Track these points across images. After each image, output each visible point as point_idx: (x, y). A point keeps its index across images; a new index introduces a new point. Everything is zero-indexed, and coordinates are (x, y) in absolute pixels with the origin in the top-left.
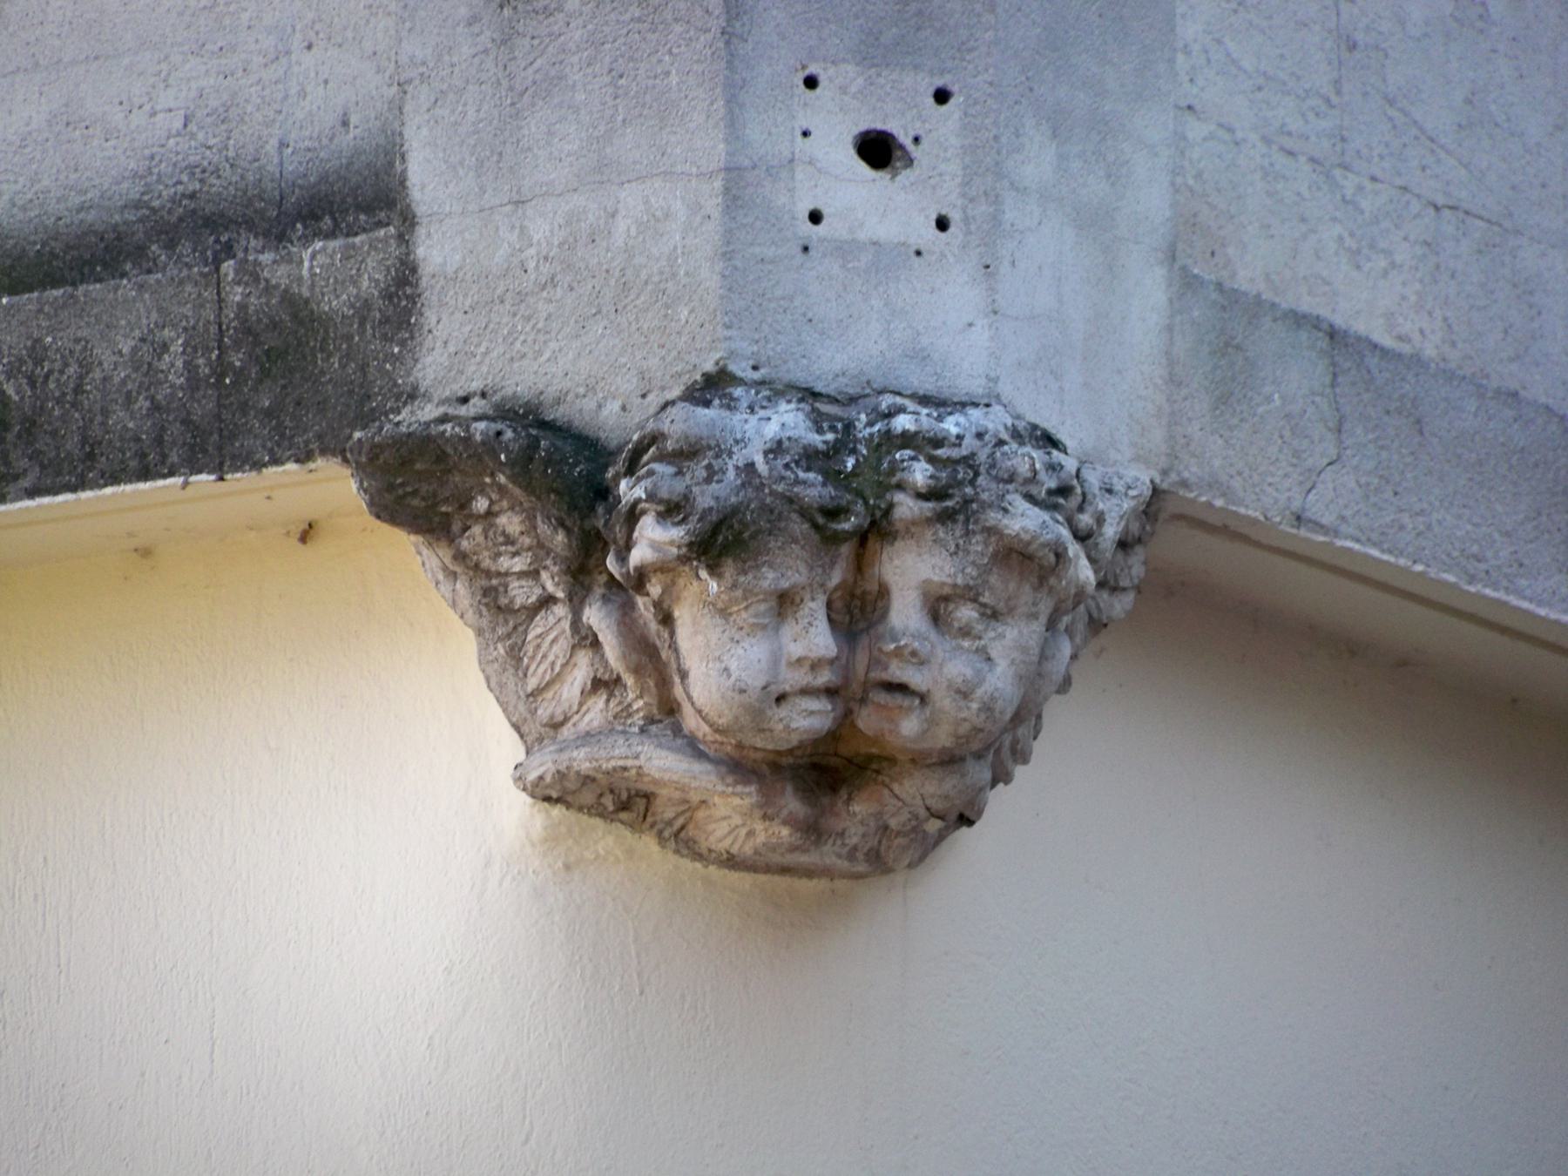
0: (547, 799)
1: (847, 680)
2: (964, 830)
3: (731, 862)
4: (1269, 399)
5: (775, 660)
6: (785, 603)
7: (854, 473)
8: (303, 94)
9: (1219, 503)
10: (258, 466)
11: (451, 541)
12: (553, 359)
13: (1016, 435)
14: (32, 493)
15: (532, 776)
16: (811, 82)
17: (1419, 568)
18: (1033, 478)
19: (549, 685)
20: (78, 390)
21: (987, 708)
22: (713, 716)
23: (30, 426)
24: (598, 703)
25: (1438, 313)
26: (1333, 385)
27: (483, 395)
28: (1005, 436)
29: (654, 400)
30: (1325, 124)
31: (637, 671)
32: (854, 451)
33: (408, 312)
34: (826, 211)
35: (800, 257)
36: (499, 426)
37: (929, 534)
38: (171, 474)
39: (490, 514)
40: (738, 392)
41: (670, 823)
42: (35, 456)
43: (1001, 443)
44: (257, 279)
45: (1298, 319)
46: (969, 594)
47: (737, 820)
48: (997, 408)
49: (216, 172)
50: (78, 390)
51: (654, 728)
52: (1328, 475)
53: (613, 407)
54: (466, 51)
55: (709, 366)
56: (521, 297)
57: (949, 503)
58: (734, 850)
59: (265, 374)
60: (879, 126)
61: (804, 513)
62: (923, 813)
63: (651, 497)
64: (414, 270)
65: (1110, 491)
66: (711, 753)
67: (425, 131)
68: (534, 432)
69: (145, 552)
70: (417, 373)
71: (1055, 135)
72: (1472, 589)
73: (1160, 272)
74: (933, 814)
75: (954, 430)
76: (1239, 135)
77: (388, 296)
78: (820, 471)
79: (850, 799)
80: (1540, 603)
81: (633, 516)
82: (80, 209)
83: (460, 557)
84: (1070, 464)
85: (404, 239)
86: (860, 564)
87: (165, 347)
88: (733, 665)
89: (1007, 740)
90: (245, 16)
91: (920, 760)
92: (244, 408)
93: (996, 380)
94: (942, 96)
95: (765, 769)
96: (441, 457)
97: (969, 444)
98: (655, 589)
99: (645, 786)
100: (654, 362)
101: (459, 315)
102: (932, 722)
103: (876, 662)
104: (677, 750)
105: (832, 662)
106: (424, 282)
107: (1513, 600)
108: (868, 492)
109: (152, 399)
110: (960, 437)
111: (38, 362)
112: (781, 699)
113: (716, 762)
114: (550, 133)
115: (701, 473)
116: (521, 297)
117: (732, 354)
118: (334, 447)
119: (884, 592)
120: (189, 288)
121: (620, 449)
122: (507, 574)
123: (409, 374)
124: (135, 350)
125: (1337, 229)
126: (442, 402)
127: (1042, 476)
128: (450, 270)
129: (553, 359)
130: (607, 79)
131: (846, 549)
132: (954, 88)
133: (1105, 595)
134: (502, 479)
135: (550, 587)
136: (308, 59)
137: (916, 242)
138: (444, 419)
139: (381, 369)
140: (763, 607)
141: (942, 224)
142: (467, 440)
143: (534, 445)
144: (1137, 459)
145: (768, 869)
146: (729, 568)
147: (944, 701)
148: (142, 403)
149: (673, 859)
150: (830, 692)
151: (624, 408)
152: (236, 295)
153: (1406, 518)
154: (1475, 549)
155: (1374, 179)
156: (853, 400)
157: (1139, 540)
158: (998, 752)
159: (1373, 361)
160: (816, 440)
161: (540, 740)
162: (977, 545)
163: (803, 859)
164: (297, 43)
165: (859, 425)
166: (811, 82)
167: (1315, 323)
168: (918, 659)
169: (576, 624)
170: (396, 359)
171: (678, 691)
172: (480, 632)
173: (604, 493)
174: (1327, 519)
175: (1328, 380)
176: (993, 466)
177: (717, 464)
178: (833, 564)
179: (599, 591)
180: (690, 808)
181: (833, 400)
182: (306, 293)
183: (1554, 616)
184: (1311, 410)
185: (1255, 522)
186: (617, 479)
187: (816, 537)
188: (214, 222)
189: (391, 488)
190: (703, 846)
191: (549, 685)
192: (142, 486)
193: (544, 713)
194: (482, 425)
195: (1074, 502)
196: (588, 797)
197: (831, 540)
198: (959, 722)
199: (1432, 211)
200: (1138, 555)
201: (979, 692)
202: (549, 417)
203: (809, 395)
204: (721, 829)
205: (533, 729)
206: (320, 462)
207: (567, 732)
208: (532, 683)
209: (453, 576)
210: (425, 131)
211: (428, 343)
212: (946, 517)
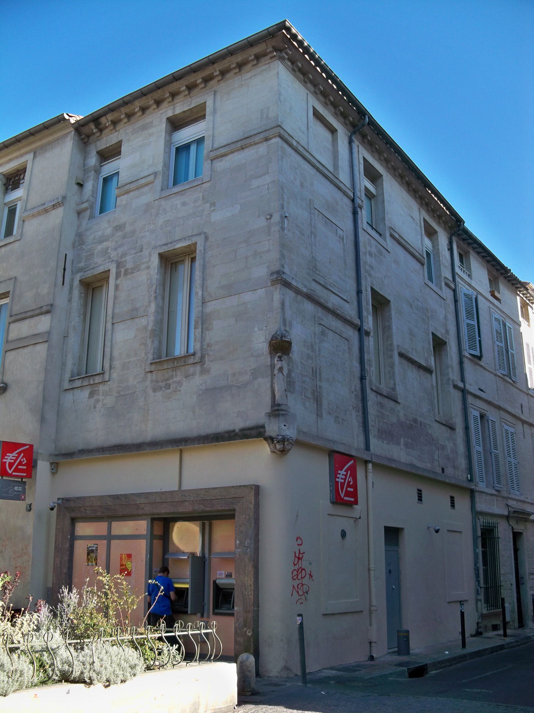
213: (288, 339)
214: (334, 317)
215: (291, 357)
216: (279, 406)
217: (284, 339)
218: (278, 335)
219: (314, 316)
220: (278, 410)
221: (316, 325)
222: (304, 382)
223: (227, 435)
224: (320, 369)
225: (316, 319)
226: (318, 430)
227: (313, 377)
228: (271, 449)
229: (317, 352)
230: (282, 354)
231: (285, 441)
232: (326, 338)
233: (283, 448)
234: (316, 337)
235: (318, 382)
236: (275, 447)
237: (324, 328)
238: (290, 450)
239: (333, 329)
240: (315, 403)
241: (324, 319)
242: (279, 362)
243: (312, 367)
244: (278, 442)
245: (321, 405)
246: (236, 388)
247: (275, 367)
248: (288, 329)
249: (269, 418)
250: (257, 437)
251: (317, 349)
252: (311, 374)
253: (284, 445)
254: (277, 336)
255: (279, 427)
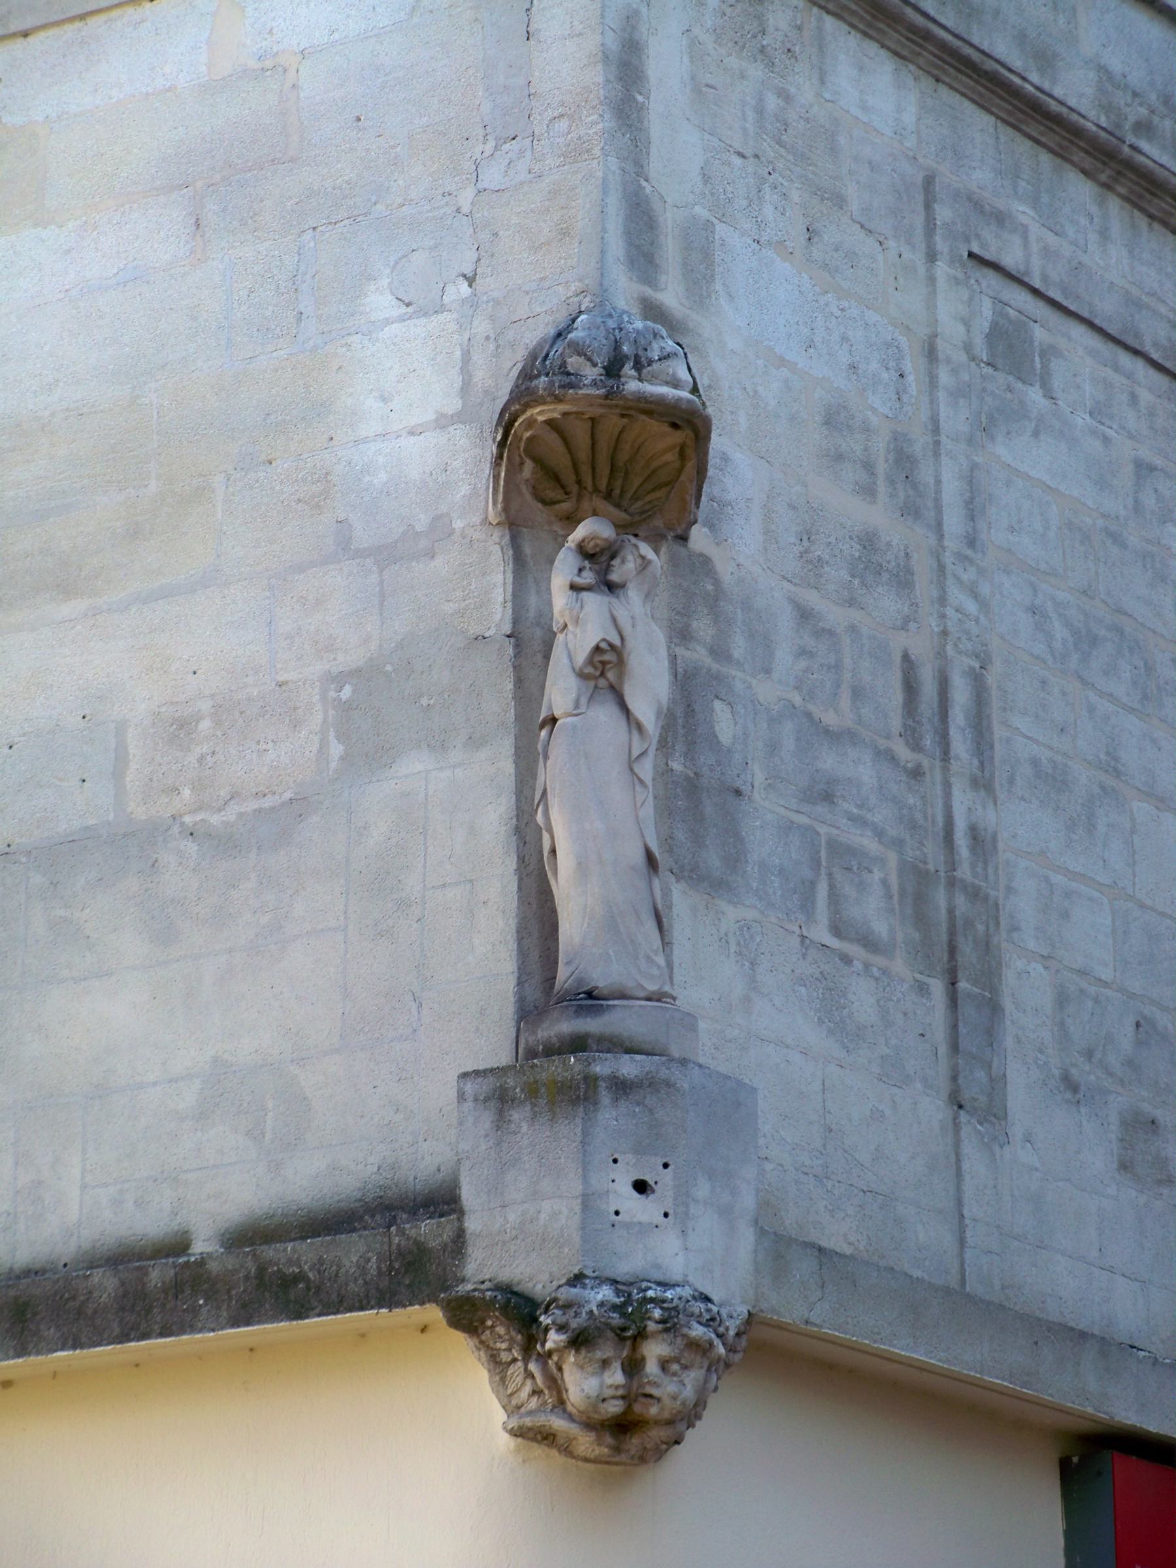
0: (516, 1435)
1: (629, 1393)
2: (676, 1447)
3: (586, 1460)
4: (795, 1276)
5: (601, 1386)
6: (605, 1364)
7: (632, 1313)
8: (423, 1158)
9: (775, 1318)
10: (405, 1306)
11: (478, 1336)
12: (517, 1267)
13: (694, 1298)
14: (319, 1315)
15: (510, 1427)
16: (615, 1161)
17: (854, 1339)
18: (701, 1314)
19: (516, 1392)
20: (336, 1276)
21: (683, 1404)
22: (575, 1404)
23: (318, 1290)
24: (535, 1399)
25: (865, 1233)
26: (820, 1269)
27: (490, 1281)
28: (690, 1298)
29: (555, 1284)
30: (820, 1162)
31: (549, 1388)
32: (632, 1305)
33: (461, 1248)
34: (621, 1211)
35: (611, 1229)
36: (495, 1294)
37: (660, 1337)
38: (372, 1308)
39: (493, 1327)
40: (587, 1281)
41: (562, 1445)
42: (320, 1301)
43: (688, 1301)
44: (404, 1234)
45: (806, 1245)
46: (677, 1360)
47: (588, 1445)
48: (687, 1287)
49: (390, 1188)
50: (336, 1276)
51: (556, 1410)
52: (818, 1305)
53: (539, 1286)
54: (483, 1147)
55: (576, 1271)
56: (504, 1243)
57: (668, 1325)
58: (588, 1456)
59: (406, 1271)
60: (642, 1178)
61: (612, 1329)
62: (659, 1442)
63: (554, 1323)
64: (464, 1231)
65: (731, 1317)
66: (577, 1420)
67: (468, 1179)
68: (509, 1296)
69: (363, 1335)
70: (465, 1272)
71: (710, 1178)
72: (876, 1346)
73: (752, 1229)
74: (665, 1443)
75: (670, 1297)
76: (786, 1168)
77: (454, 1242)
78: (618, 1313)
79: (631, 1438)
80: (902, 1349)
81: (547, 1330)
82: (338, 1202)
83: (482, 1342)
84: (715, 1309)
85: (460, 1219)
86: (634, 1348)
87: (369, 1260)
88: (586, 1388)
89: (693, 1412)
90: (401, 1128)
91: (657, 1423)
92: (399, 1283)
93: (687, 1276)
94: (666, 1166)
95: (599, 1426)
96: (474, 1305)
97: (676, 1301)
98: (555, 1358)
99: (552, 1431)
100: (555, 1269)
101: (481, 1249)
102: (662, 1409)
103: (641, 1385)
104: (564, 1419)
105: (623, 1386)
106: (467, 1236)
107: (892, 1349)
108: (637, 1320)
109: (364, 1280)
110: (672, 1299)
111: (322, 1265)
112: (604, 1400)
113: (579, 1423)
114: (516, 1180)
115: (572, 1314)
116: (504, 1243)
117: (585, 1266)
118: (433, 1299)
119: (643, 1359)
120: (378, 1237)
121: (542, 1303)
122: (499, 1349)
123: (462, 1271)
124: (358, 1261)
125: (825, 1202)
126: (474, 1283)
127: (704, 1314)
128: (477, 1233)
129: (517, 1267)
130: (537, 1160)
131: (629, 1343)
132: (670, 1163)
133: (731, 1354)
134: (497, 1314)
135: (516, 1355)
136: (425, 1145)
137: (655, 1223)
138: (475, 1290)
139: (451, 1269)
140: (596, 1365)
141: (666, 1215)
142: (484, 1299)
143: (509, 1301)
144: (743, 1302)
145: (600, 1462)
146: (583, 1352)
147: (667, 1401)
148: (361, 1281)
149: (564, 1459)
150: (623, 1397)
151: (544, 1287)
152: (396, 1240)
153: (849, 1320)
154: (876, 1330)
155: (839, 1182)
156: (631, 1284)
157: (744, 1333)
158: (689, 1417)
159: (836, 1259)
160: (617, 1301)
161: (513, 1412)
162: (679, 1340)
163: (614, 1460)
164: (421, 1138)
165: (634, 1294)
166: (615, 1161)
167: (813, 1245)
168: (656, 1384)
169: (526, 1369)
170: (457, 1266)
171: (565, 1396)
172: (489, 1371)
173: (535, 1320)
174: (818, 1322)
175: (818, 1268)
176: (685, 1310)
177: (579, 1311)
178: (623, 1349)
179: (534, 1357)
180: (570, 1440)
181: (624, 1284)
182: (423, 1240)
183: (908, 1354)
184: (811, 1280)
185: (790, 1324)
186: (541, 1315)
187: (616, 1339)
188: (389, 1208)
189: (455, 1316)
190: (576, 1454)
191: (516, 1392)
192: (362, 1313)
193: (514, 1402)
194: (489, 1293)
195: (717, 1323)
196: (531, 1435)
197: (623, 1339)
198: (673, 1409)
199: (862, 1193)
200: (744, 1337)
201: (680, 1397)
202: (516, 1289)
203: (614, 1282)
204: (582, 1448)
205: (509, 1408)
206: (427, 1305)
207: (523, 1410)
208: (509, 1391)
209: (479, 1349)
210: (468, 1179)
211: (469, 1260)
212: (667, 1330)
213: (676, 384)
214: (1114, 205)
215: (706, 561)
216: (580, 1011)
217: (632, 386)
218: (579, 350)
219: (929, 182)
220: (578, 1044)
221: (942, 269)
222: (828, 797)
223: (105, 1283)
224: (978, 681)
225: (943, 213)
226: (962, 1242)
227: (916, 747)
228: (512, 1409)
229: (954, 521)
230: (620, 527)
231: (641, 1335)
232: (1034, 395)
233: (627, 1398)
234: (944, 377)
235: (962, 800)
236: (555, 1384)
237: (1020, 298)
238: (691, 1415)
239: (1106, 309)
240: (938, 987)
241: (1022, 211)
242: (594, 602)
243: (906, 657)
244: (579, 1341)
245: (994, 1008)
246: (191, 847)
247: (558, 652)
248: (671, 297)
249: (501, 1121)
250: (387, 1298)
251: (952, 489)
252: (896, 722)
253: (633, 1367)
254: (573, 362)
255: (588, 1202)
